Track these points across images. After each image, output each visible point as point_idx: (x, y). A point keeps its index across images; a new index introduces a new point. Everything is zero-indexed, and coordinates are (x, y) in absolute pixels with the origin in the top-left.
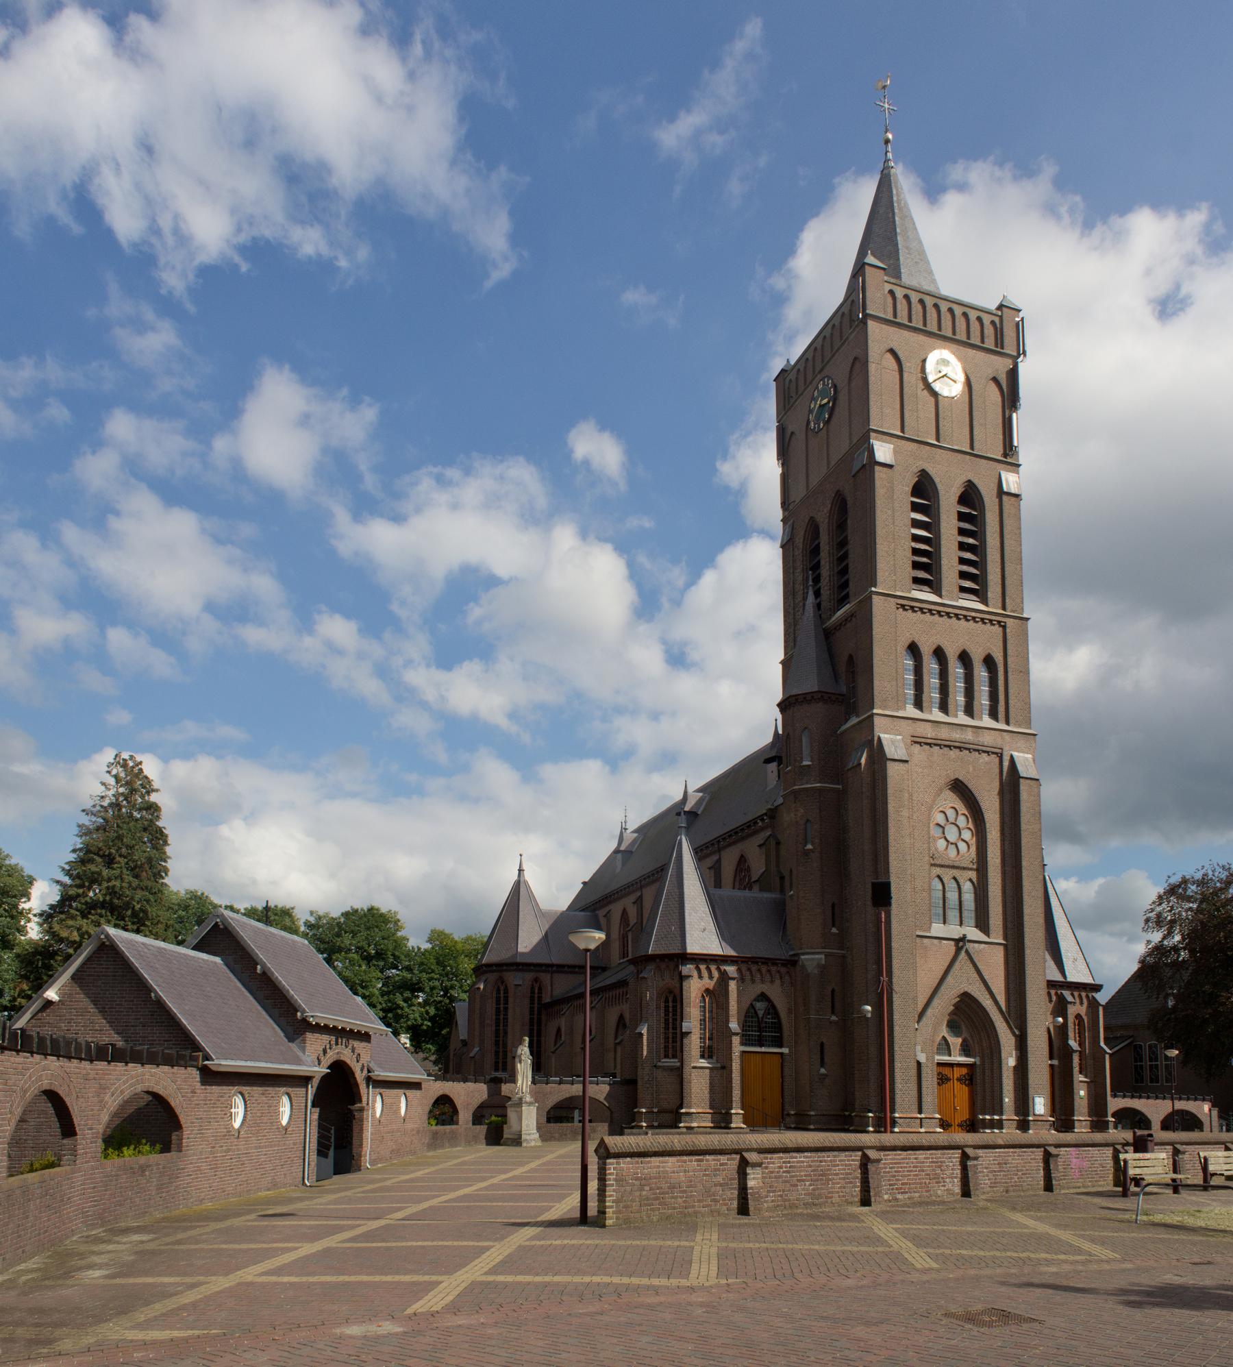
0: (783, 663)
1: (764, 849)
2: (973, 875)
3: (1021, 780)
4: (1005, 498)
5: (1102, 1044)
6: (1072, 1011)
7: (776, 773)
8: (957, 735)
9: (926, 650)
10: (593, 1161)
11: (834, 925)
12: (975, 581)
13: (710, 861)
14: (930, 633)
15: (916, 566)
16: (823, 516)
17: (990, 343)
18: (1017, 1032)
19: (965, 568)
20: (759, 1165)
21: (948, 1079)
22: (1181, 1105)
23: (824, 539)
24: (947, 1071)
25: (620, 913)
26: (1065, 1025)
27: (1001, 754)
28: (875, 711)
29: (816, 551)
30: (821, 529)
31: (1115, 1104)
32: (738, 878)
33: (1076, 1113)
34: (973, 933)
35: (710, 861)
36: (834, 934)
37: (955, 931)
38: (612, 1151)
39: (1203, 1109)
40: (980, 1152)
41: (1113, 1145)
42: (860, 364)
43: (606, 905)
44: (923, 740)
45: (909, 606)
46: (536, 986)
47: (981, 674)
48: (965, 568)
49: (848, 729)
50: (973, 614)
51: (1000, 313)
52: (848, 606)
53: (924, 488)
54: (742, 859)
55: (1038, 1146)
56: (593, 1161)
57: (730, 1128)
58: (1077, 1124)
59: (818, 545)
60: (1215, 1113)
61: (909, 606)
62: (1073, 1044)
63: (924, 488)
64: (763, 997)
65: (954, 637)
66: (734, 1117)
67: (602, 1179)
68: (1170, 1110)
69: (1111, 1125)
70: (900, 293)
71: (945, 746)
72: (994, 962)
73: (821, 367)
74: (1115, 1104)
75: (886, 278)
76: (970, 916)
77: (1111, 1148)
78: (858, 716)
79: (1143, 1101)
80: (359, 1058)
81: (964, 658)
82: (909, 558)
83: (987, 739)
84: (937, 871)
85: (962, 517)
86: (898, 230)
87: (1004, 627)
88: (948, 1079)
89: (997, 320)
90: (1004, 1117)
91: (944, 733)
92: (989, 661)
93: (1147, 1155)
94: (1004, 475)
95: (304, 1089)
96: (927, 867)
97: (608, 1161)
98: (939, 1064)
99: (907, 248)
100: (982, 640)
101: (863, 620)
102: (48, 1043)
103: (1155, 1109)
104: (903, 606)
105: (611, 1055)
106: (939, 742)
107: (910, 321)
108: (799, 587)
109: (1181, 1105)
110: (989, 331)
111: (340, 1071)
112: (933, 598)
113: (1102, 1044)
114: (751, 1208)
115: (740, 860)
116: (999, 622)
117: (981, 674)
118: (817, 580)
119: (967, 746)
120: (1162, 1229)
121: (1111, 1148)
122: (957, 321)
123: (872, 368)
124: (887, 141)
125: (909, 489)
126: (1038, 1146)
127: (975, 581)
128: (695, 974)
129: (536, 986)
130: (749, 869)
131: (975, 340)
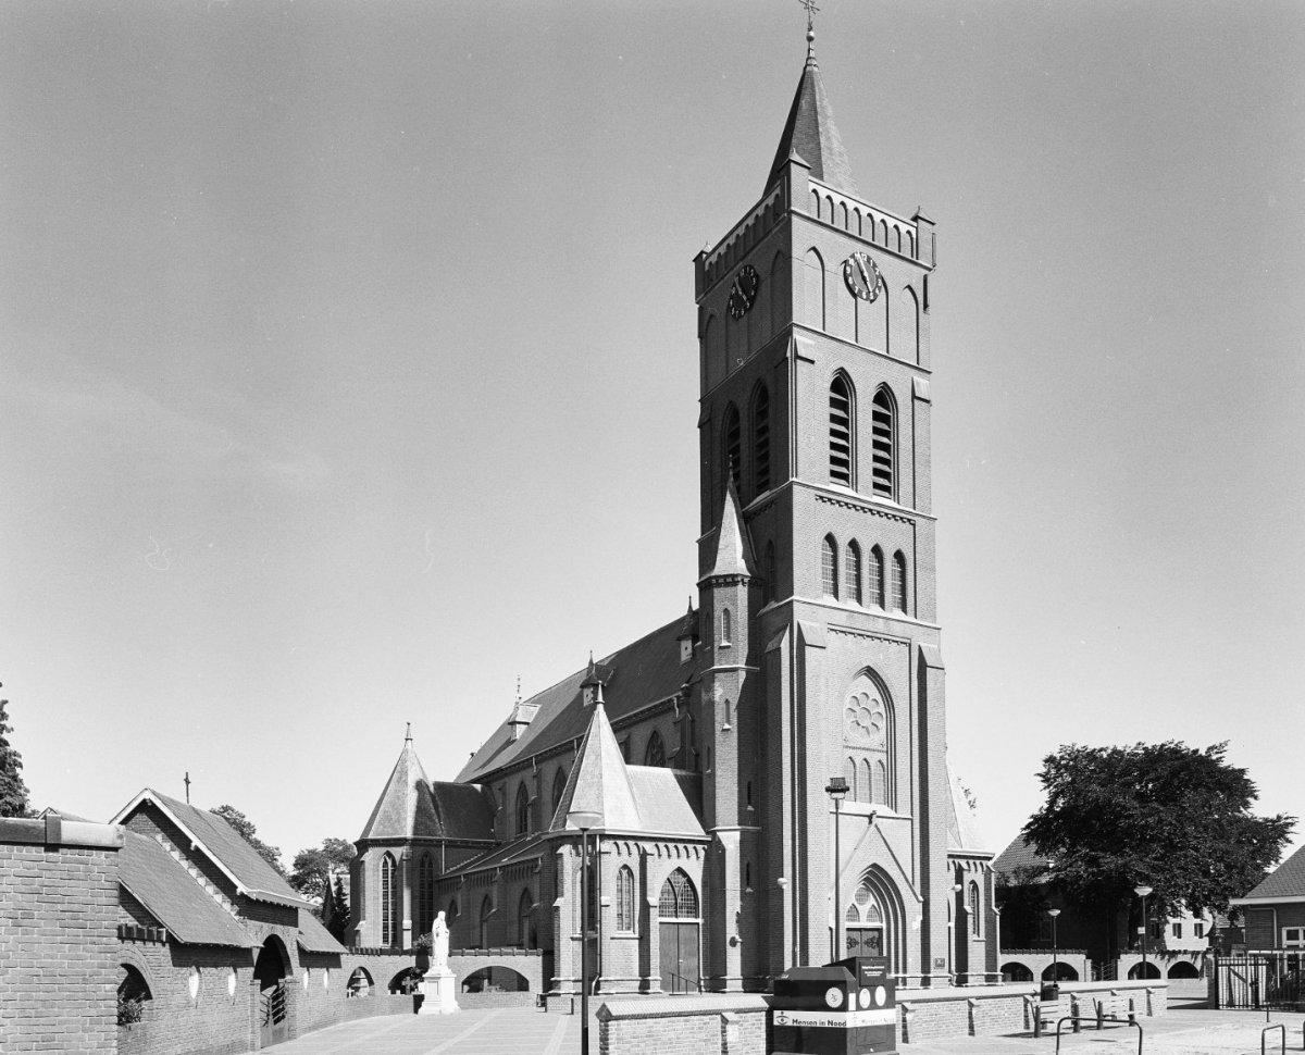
0: (700, 542)
1: (679, 726)
2: (883, 757)
3: (928, 669)
4: (916, 401)
5: (994, 908)
6: (967, 877)
7: (690, 650)
8: (870, 626)
10: (594, 1025)
11: (749, 803)
12: (885, 478)
13: (624, 736)
15: (834, 460)
16: (743, 403)
17: (906, 253)
18: (921, 899)
19: (879, 466)
20: (913, 1011)
21: (857, 943)
22: (1062, 958)
23: (744, 424)
24: (855, 935)
25: (517, 788)
26: (962, 891)
27: (910, 645)
28: (794, 597)
29: (735, 435)
30: (741, 415)
31: (1003, 959)
32: (650, 755)
33: (969, 968)
34: (884, 810)
35: (624, 736)
36: (750, 811)
37: (867, 809)
38: (614, 1014)
39: (1077, 960)
40: (916, 1006)
41: (1022, 995)
42: (783, 259)
43: (502, 778)
44: (858, 632)
46: (427, 860)
47: (890, 565)
48: (879, 466)
49: (767, 613)
51: (915, 224)
52: (767, 493)
53: (842, 385)
54: (655, 735)
55: (963, 999)
56: (594, 1025)
57: (648, 994)
58: (970, 978)
59: (738, 429)
60: (1089, 962)
62: (968, 908)
63: (842, 385)
64: (680, 870)
65: (869, 532)
66: (651, 983)
67: (604, 1039)
68: (1052, 962)
69: (1000, 978)
70: (823, 193)
71: (859, 635)
72: (902, 837)
73: (742, 254)
74: (1003, 959)
75: (811, 178)
76: (879, 788)
77: (719, 1017)
78: (777, 601)
79: (1027, 956)
80: (289, 937)
81: (877, 550)
82: (828, 452)
84: (850, 753)
85: (877, 416)
87: (914, 525)
88: (857, 943)
89: (913, 231)
90: (931, 975)
92: (899, 556)
93: (1054, 1002)
96: (840, 749)
97: (610, 1023)
100: (893, 538)
101: (783, 505)
102: (135, 931)
103: (1037, 962)
104: (821, 498)
105: (515, 927)
106: (853, 631)
107: (833, 222)
108: (717, 469)
109: (1062, 958)
110: (906, 239)
111: (273, 946)
112: (849, 491)
113: (994, 908)
114: (910, 1040)
115: (653, 736)
116: (909, 520)
117: (890, 565)
118: (737, 462)
119: (879, 635)
121: (719, 1017)
122: (876, 226)
123: (795, 264)
124: (810, 39)
125: (829, 385)
126: (963, 999)
127: (885, 478)
128: (655, 851)
129: (427, 860)
130: (661, 747)
131: (893, 248)
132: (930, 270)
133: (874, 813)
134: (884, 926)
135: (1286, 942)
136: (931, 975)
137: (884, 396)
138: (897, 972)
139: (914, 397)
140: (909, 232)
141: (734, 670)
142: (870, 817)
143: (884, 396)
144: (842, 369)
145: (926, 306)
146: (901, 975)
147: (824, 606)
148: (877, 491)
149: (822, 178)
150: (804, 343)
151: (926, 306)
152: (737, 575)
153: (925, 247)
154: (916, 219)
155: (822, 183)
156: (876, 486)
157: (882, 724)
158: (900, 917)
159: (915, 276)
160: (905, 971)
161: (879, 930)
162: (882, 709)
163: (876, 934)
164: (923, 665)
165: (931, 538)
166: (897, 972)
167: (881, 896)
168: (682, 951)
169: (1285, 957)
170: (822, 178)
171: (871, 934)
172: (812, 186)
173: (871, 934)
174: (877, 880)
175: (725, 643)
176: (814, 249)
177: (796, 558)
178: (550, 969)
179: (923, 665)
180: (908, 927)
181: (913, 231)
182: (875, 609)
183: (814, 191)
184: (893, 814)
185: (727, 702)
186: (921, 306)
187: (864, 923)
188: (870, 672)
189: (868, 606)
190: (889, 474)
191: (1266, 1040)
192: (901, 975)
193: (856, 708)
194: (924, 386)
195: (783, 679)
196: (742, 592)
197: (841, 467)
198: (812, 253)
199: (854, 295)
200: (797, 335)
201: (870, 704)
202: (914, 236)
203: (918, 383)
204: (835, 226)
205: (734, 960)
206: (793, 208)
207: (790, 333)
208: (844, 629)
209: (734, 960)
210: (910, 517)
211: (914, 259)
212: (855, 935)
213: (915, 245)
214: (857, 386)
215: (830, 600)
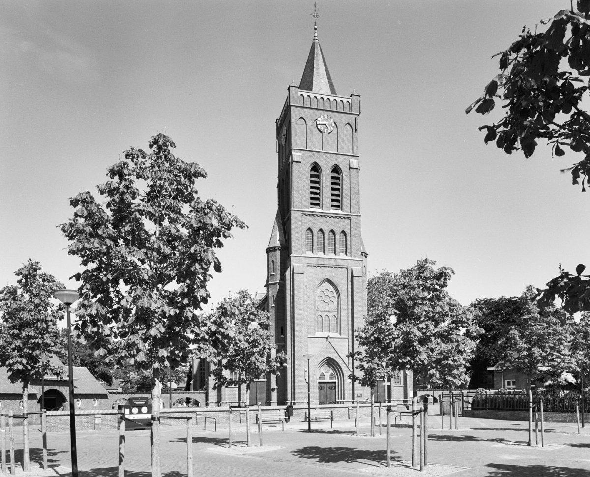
2: (336, 314)
9: (315, 230)
12: (337, 202)
14: (316, 224)
24: (323, 385)
33: (392, 397)
44: (313, 265)
45: (306, 214)
50: (336, 216)
51: (351, 98)
53: (316, 168)
61: (306, 214)
63: (316, 168)
75: (299, 90)
83: (340, 263)
84: (320, 313)
86: (314, 66)
91: (322, 262)
94: (351, 160)
95: (528, 422)
98: (319, 383)
99: (318, 73)
104: (305, 214)
112: (340, 212)
120: (340, 430)
126: (347, 407)
127: (337, 202)
132: (359, 115)
133: (328, 337)
134: (337, 381)
135: (507, 386)
136: (408, 399)
137: (336, 169)
138: (341, 399)
139: (350, 168)
140: (348, 102)
141: (275, 284)
142: (327, 338)
143: (336, 169)
144: (336, 164)
145: (356, 130)
146: (342, 400)
147: (305, 257)
148: (312, 206)
149: (335, 94)
150: (297, 155)
151: (356, 130)
152: (276, 247)
153: (355, 107)
154: (351, 96)
155: (336, 96)
156: (333, 206)
157: (335, 301)
158: (339, 378)
159: (351, 119)
160: (344, 399)
161: (335, 383)
162: (335, 294)
163: (334, 384)
164: (352, 276)
165: (359, 224)
166: (341, 399)
167: (334, 369)
168: (258, 391)
169: (387, 402)
170: (335, 94)
171: (331, 385)
172: (300, 93)
173: (331, 385)
174: (330, 362)
175: (273, 273)
176: (348, 124)
177: (292, 239)
178: (207, 399)
179: (352, 276)
180: (345, 382)
181: (350, 101)
182: (332, 255)
183: (302, 95)
184: (339, 336)
185: (273, 296)
186: (354, 130)
187: (327, 380)
188: (328, 281)
189: (339, 255)
190: (339, 200)
191: (412, 441)
192: (293, 401)
193: (323, 295)
194: (354, 163)
195: (287, 287)
196: (278, 253)
197: (316, 200)
198: (348, 125)
199: (321, 132)
200: (294, 153)
201: (331, 295)
202: (350, 103)
203: (352, 162)
204: (305, 106)
205: (274, 395)
206: (291, 104)
207: (290, 153)
208: (315, 265)
209: (274, 395)
210: (348, 217)
211: (351, 112)
212: (323, 385)
213: (351, 106)
214: (341, 168)
215: (309, 254)
